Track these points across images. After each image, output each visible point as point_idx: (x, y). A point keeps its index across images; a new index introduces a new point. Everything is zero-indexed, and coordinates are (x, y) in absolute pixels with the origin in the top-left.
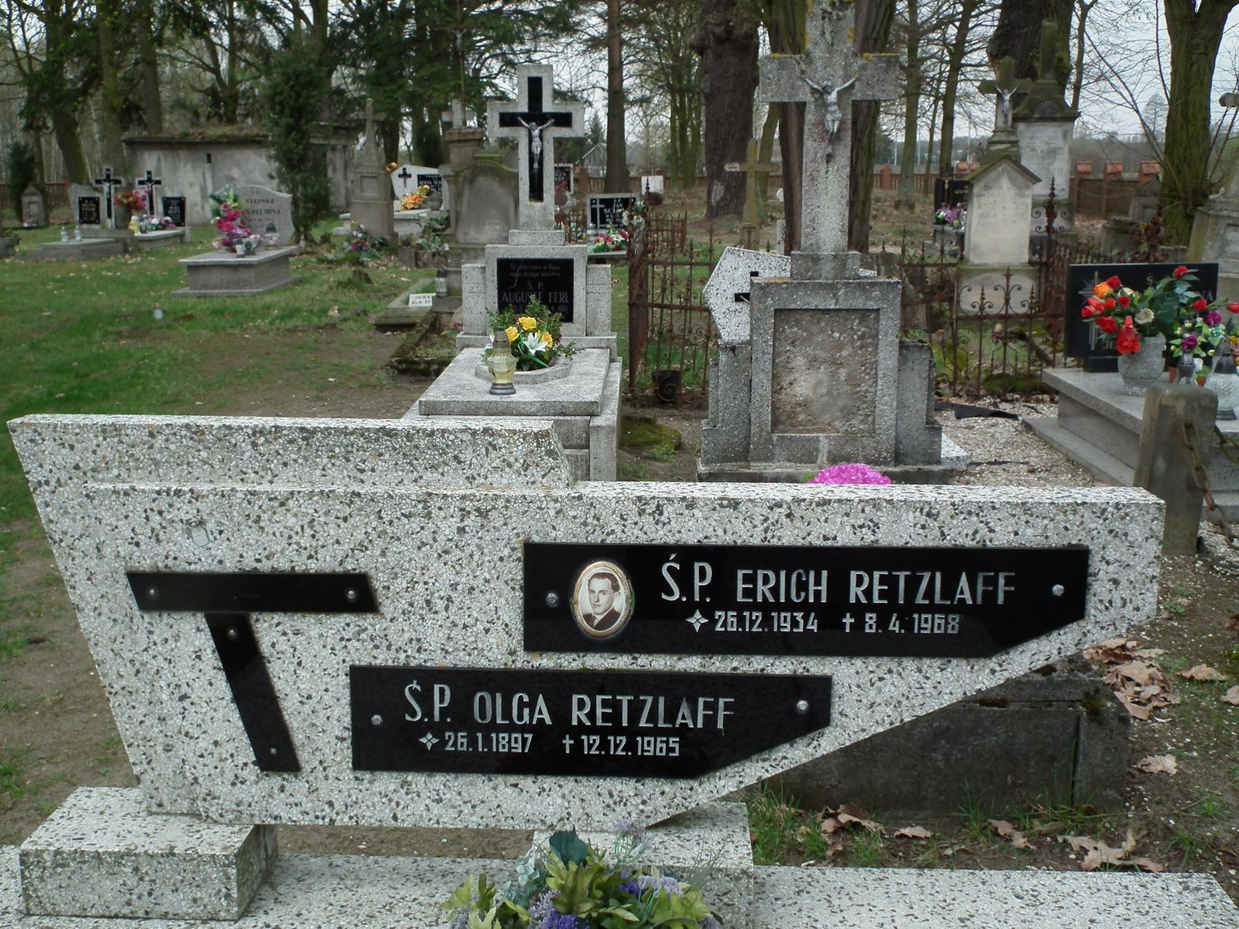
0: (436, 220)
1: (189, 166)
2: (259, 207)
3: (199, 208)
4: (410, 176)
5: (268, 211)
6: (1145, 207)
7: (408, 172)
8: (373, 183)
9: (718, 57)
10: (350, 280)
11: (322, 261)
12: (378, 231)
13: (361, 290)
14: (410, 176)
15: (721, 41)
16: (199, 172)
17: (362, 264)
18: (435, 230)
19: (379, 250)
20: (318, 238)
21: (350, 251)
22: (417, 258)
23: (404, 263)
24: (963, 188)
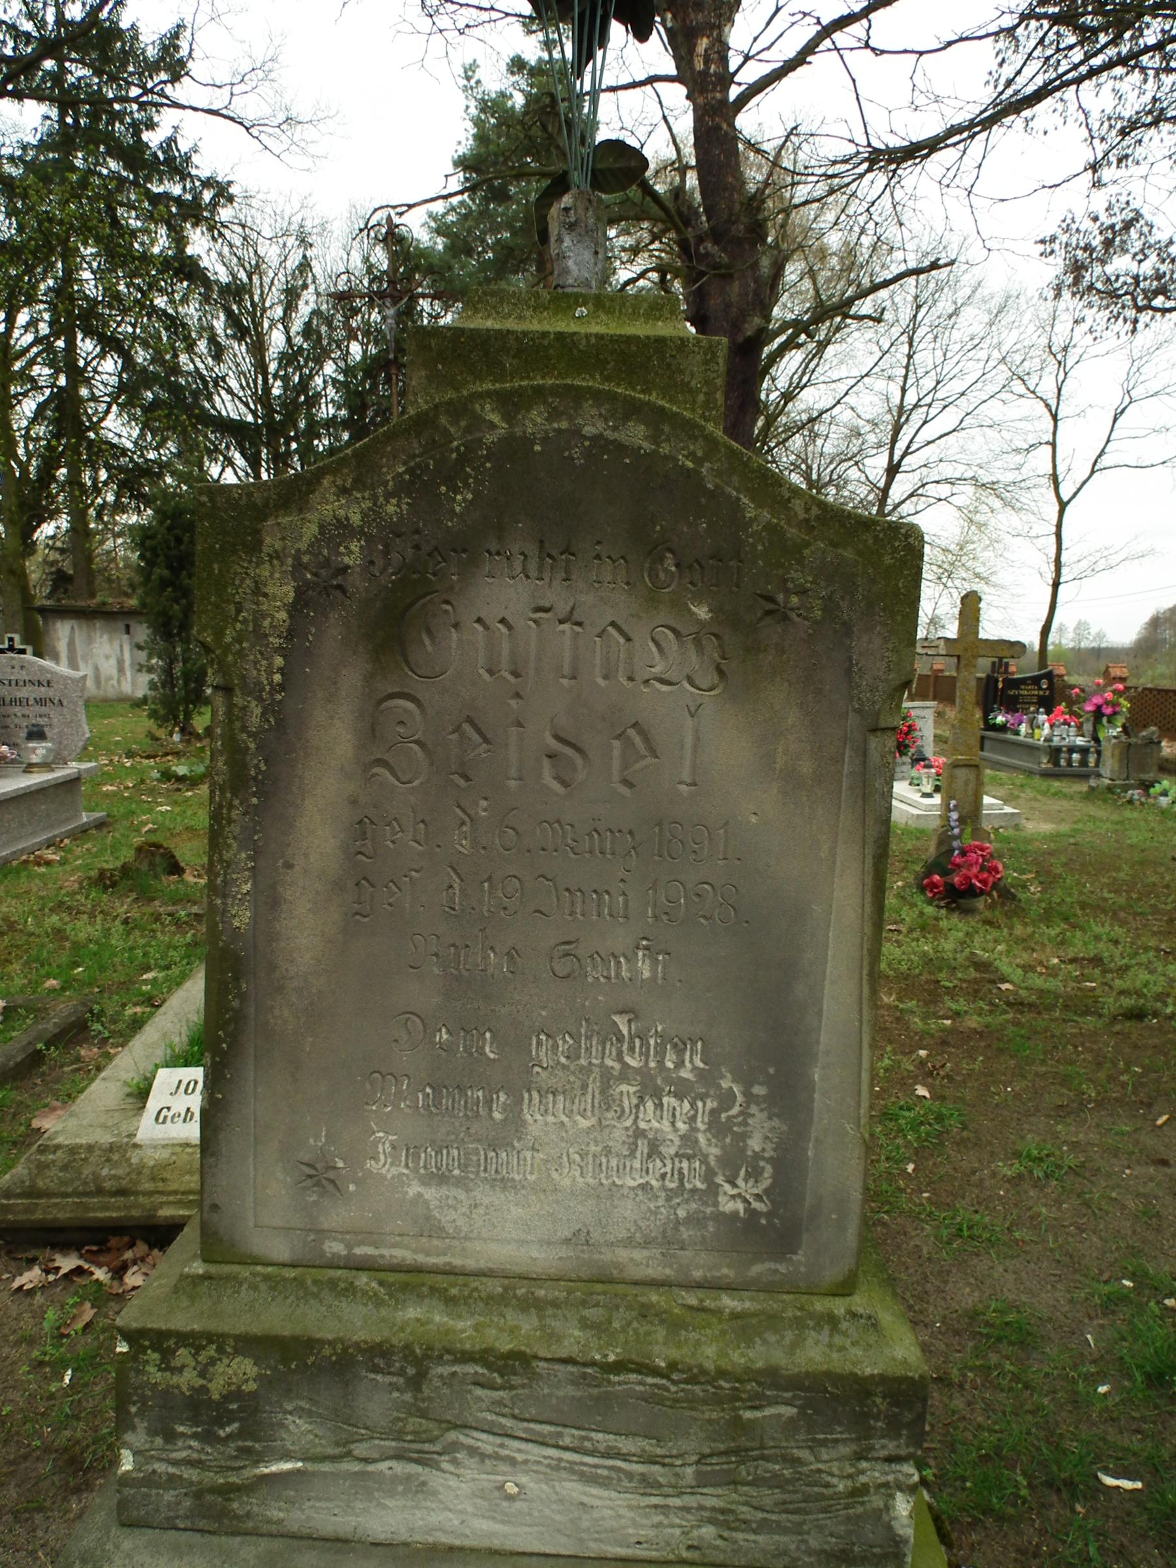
1: (105, 637)
2: (24, 693)
3: (115, 682)
5: (40, 702)
10: (125, 870)
11: (167, 776)
13: (145, 896)
16: (116, 644)
24: (1018, 688)
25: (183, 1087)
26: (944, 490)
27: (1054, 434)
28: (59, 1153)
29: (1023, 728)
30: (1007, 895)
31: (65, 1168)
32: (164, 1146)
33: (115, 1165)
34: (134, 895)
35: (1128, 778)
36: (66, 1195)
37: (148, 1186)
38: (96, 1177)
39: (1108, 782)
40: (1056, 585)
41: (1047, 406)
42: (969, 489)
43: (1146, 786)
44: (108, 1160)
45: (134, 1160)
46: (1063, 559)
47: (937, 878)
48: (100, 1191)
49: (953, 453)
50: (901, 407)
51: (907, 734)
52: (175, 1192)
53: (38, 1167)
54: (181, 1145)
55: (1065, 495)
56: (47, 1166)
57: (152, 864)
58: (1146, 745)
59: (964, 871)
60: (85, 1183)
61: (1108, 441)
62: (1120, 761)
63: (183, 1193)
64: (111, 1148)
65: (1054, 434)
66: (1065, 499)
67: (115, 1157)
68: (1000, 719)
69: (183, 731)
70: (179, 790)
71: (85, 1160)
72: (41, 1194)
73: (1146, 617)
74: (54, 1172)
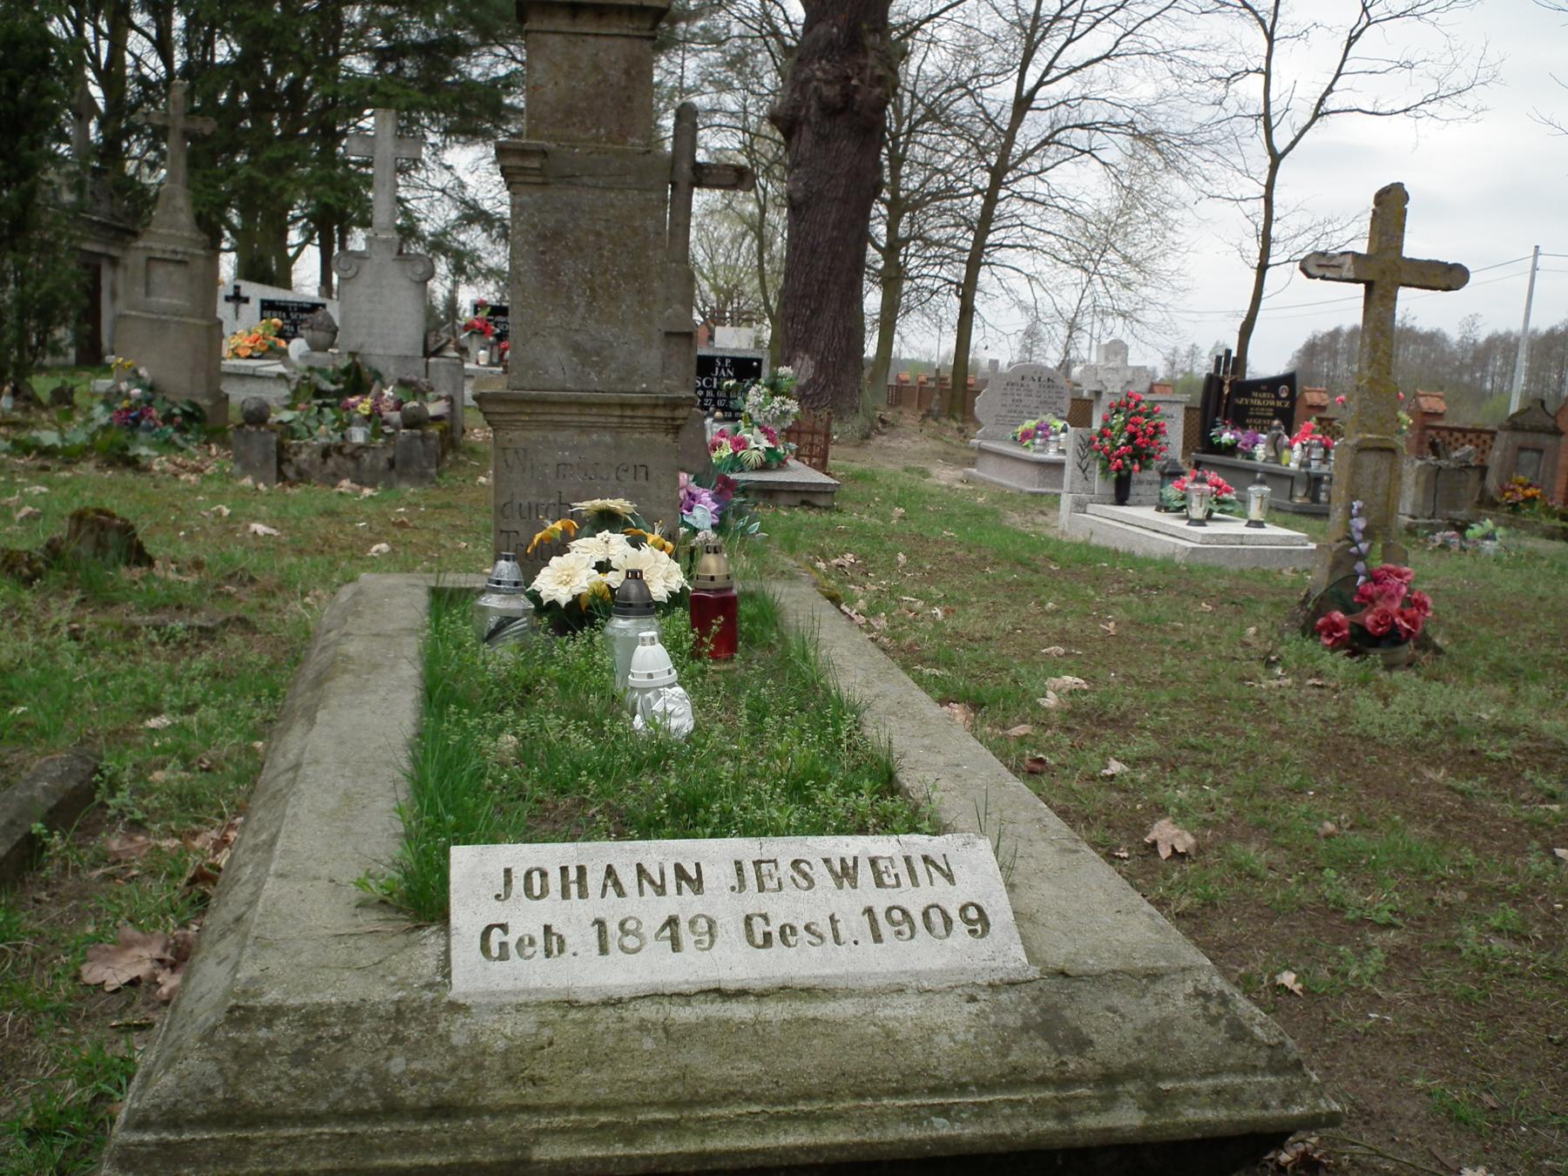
0: (322, 371)
4: (246, 300)
6: (1522, 449)
7: (244, 292)
8: (178, 275)
9: (822, 139)
10: (53, 549)
12: (181, 386)
13: (98, 597)
14: (246, 300)
15: (830, 111)
17: (133, 463)
18: (319, 393)
19: (181, 429)
20: (45, 397)
21: (105, 428)
22: (282, 456)
23: (248, 468)
24: (1249, 396)
25: (518, 884)
26: (1080, 138)
27: (1269, 58)
28: (280, 1026)
29: (1260, 451)
30: (1425, 644)
31: (301, 1057)
32: (519, 1008)
33: (416, 1050)
34: (76, 595)
35: (1433, 516)
36: (313, 1119)
37: (503, 1095)
38: (381, 1078)
39: (1407, 520)
40: (1262, 268)
41: (1262, 22)
42: (1123, 141)
43: (1461, 528)
44: (397, 1039)
45: (458, 1039)
46: (1274, 233)
47: (1338, 616)
48: (392, 1109)
49: (1096, 89)
50: (1036, 16)
51: (1153, 437)
52: (563, 1108)
53: (236, 1056)
54: (556, 1005)
55: (1280, 144)
56: (259, 1055)
57: (100, 545)
58: (1461, 470)
59: (1381, 605)
60: (357, 1092)
61: (1338, 74)
62: (1426, 491)
63: (582, 1109)
64: (400, 1013)
65: (1269, 58)
66: (1280, 150)
67: (413, 1032)
68: (1227, 437)
69: (15, 392)
70: (45, 469)
71: (343, 1039)
72: (252, 1118)
73: (1300, 342)
74: (277, 1066)
